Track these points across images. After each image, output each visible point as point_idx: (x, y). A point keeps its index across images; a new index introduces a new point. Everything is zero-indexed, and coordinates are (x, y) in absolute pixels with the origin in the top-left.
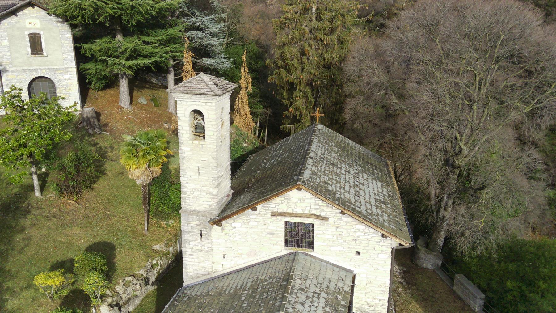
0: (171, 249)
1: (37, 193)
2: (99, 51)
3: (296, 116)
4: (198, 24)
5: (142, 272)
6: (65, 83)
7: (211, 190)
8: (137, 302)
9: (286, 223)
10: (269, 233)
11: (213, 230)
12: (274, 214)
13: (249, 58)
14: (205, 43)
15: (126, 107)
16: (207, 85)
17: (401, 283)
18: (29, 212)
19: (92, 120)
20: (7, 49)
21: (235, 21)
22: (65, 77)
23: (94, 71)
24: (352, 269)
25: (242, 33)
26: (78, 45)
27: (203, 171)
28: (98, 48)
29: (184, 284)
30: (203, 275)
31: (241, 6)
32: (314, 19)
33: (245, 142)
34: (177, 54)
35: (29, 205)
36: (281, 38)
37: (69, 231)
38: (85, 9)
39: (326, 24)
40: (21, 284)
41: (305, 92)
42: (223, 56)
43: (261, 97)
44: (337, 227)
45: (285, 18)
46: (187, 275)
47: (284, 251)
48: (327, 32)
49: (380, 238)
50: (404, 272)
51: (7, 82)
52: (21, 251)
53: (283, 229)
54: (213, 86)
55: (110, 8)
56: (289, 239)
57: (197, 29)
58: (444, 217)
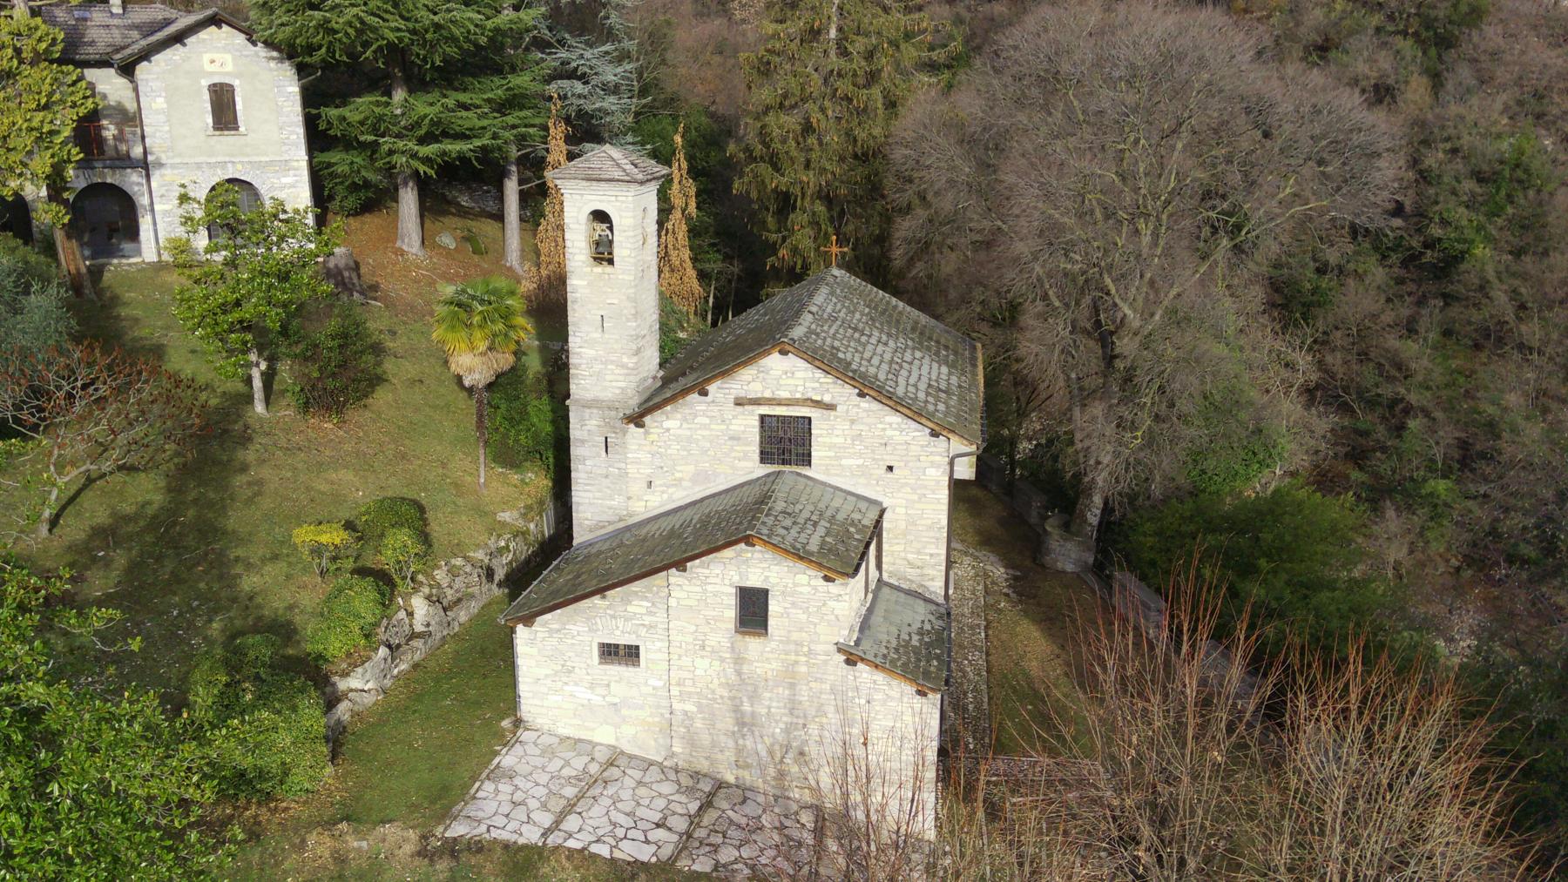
0: (532, 526)
1: (259, 407)
2: (362, 123)
3: (794, 268)
4: (574, 64)
5: (480, 555)
8: (474, 607)
9: (763, 418)
10: (732, 438)
11: (628, 436)
12: (739, 402)
13: (690, 144)
14: (589, 107)
15: (414, 250)
16: (618, 165)
17: (1007, 595)
18: (250, 439)
19: (346, 274)
20: (162, 118)
21: (656, 60)
22: (284, 180)
23: (346, 168)
25: (670, 87)
26: (314, 111)
27: (615, 317)
28: (358, 117)
29: (575, 543)
31: (668, 23)
32: (833, 54)
33: (683, 329)
34: (531, 130)
35: (247, 427)
36: (765, 94)
38: (336, 32)
39: (859, 64)
40: (260, 553)
41: (814, 214)
42: (629, 138)
43: (717, 234)
44: (853, 422)
45: (768, 51)
46: (580, 525)
47: (763, 470)
48: (861, 81)
49: (928, 438)
50: (1016, 578)
51: (163, 191)
52: (250, 501)
53: (757, 430)
54: (629, 167)
55: (392, 29)
57: (572, 75)
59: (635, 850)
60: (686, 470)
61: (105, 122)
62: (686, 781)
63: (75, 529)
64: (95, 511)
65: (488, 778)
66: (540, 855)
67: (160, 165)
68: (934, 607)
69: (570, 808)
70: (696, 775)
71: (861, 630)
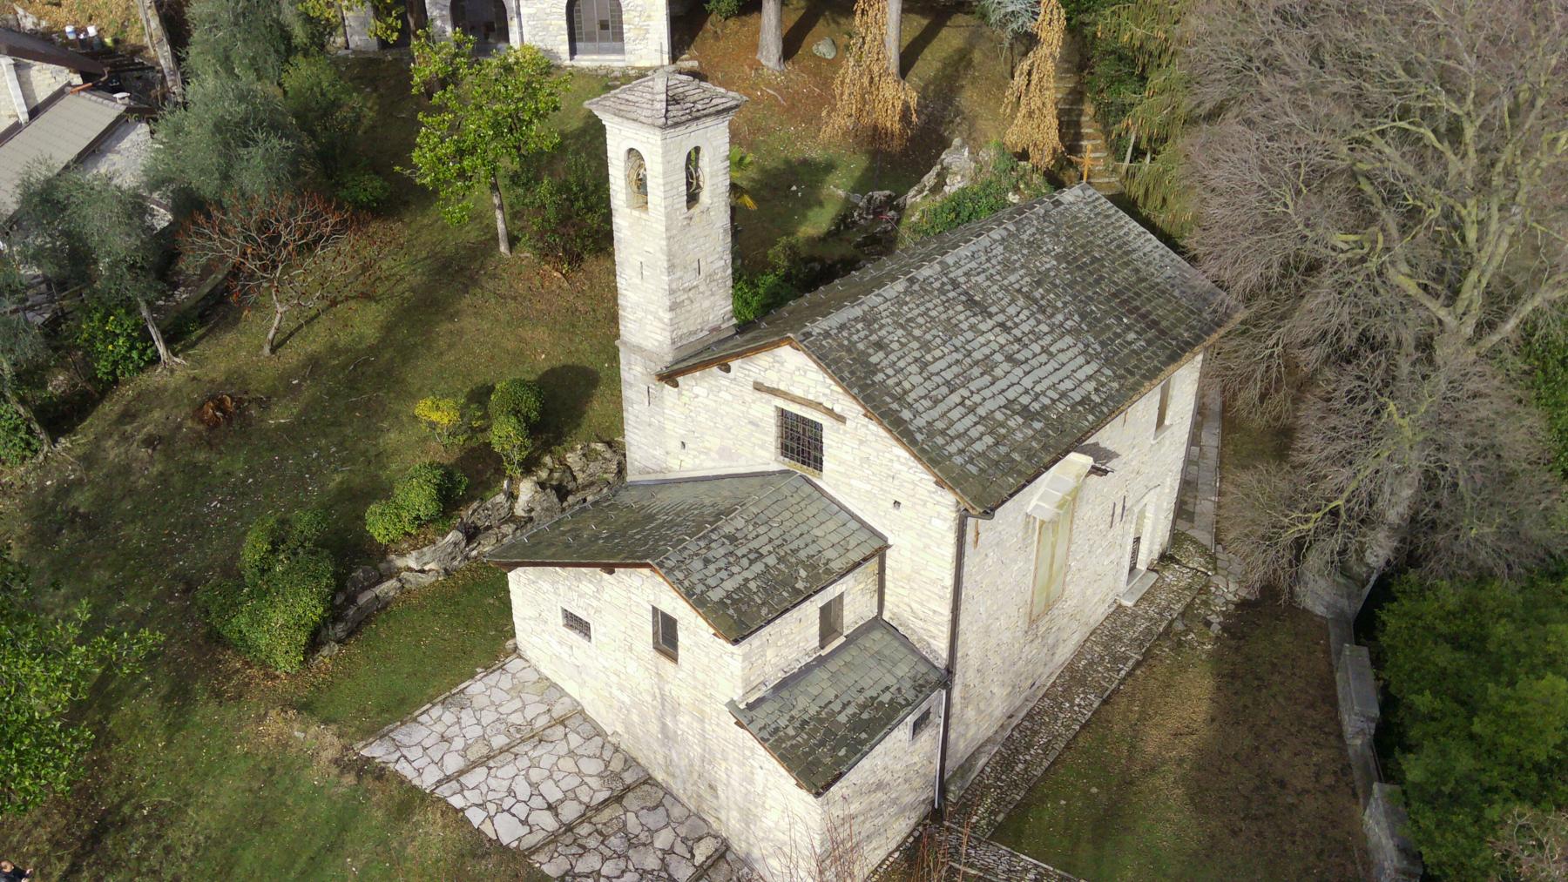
1: (503, 248)
7: (661, 313)
12: (758, 387)
24: (886, 533)
30: (655, 472)
33: (1016, 190)
37: (527, 333)
44: (861, 442)
56: (789, 443)
59: (507, 831)
60: (713, 442)
62: (616, 765)
63: (293, 354)
64: (314, 342)
66: (423, 800)
68: (923, 669)
69: (484, 761)
70: (630, 762)
71: (778, 688)
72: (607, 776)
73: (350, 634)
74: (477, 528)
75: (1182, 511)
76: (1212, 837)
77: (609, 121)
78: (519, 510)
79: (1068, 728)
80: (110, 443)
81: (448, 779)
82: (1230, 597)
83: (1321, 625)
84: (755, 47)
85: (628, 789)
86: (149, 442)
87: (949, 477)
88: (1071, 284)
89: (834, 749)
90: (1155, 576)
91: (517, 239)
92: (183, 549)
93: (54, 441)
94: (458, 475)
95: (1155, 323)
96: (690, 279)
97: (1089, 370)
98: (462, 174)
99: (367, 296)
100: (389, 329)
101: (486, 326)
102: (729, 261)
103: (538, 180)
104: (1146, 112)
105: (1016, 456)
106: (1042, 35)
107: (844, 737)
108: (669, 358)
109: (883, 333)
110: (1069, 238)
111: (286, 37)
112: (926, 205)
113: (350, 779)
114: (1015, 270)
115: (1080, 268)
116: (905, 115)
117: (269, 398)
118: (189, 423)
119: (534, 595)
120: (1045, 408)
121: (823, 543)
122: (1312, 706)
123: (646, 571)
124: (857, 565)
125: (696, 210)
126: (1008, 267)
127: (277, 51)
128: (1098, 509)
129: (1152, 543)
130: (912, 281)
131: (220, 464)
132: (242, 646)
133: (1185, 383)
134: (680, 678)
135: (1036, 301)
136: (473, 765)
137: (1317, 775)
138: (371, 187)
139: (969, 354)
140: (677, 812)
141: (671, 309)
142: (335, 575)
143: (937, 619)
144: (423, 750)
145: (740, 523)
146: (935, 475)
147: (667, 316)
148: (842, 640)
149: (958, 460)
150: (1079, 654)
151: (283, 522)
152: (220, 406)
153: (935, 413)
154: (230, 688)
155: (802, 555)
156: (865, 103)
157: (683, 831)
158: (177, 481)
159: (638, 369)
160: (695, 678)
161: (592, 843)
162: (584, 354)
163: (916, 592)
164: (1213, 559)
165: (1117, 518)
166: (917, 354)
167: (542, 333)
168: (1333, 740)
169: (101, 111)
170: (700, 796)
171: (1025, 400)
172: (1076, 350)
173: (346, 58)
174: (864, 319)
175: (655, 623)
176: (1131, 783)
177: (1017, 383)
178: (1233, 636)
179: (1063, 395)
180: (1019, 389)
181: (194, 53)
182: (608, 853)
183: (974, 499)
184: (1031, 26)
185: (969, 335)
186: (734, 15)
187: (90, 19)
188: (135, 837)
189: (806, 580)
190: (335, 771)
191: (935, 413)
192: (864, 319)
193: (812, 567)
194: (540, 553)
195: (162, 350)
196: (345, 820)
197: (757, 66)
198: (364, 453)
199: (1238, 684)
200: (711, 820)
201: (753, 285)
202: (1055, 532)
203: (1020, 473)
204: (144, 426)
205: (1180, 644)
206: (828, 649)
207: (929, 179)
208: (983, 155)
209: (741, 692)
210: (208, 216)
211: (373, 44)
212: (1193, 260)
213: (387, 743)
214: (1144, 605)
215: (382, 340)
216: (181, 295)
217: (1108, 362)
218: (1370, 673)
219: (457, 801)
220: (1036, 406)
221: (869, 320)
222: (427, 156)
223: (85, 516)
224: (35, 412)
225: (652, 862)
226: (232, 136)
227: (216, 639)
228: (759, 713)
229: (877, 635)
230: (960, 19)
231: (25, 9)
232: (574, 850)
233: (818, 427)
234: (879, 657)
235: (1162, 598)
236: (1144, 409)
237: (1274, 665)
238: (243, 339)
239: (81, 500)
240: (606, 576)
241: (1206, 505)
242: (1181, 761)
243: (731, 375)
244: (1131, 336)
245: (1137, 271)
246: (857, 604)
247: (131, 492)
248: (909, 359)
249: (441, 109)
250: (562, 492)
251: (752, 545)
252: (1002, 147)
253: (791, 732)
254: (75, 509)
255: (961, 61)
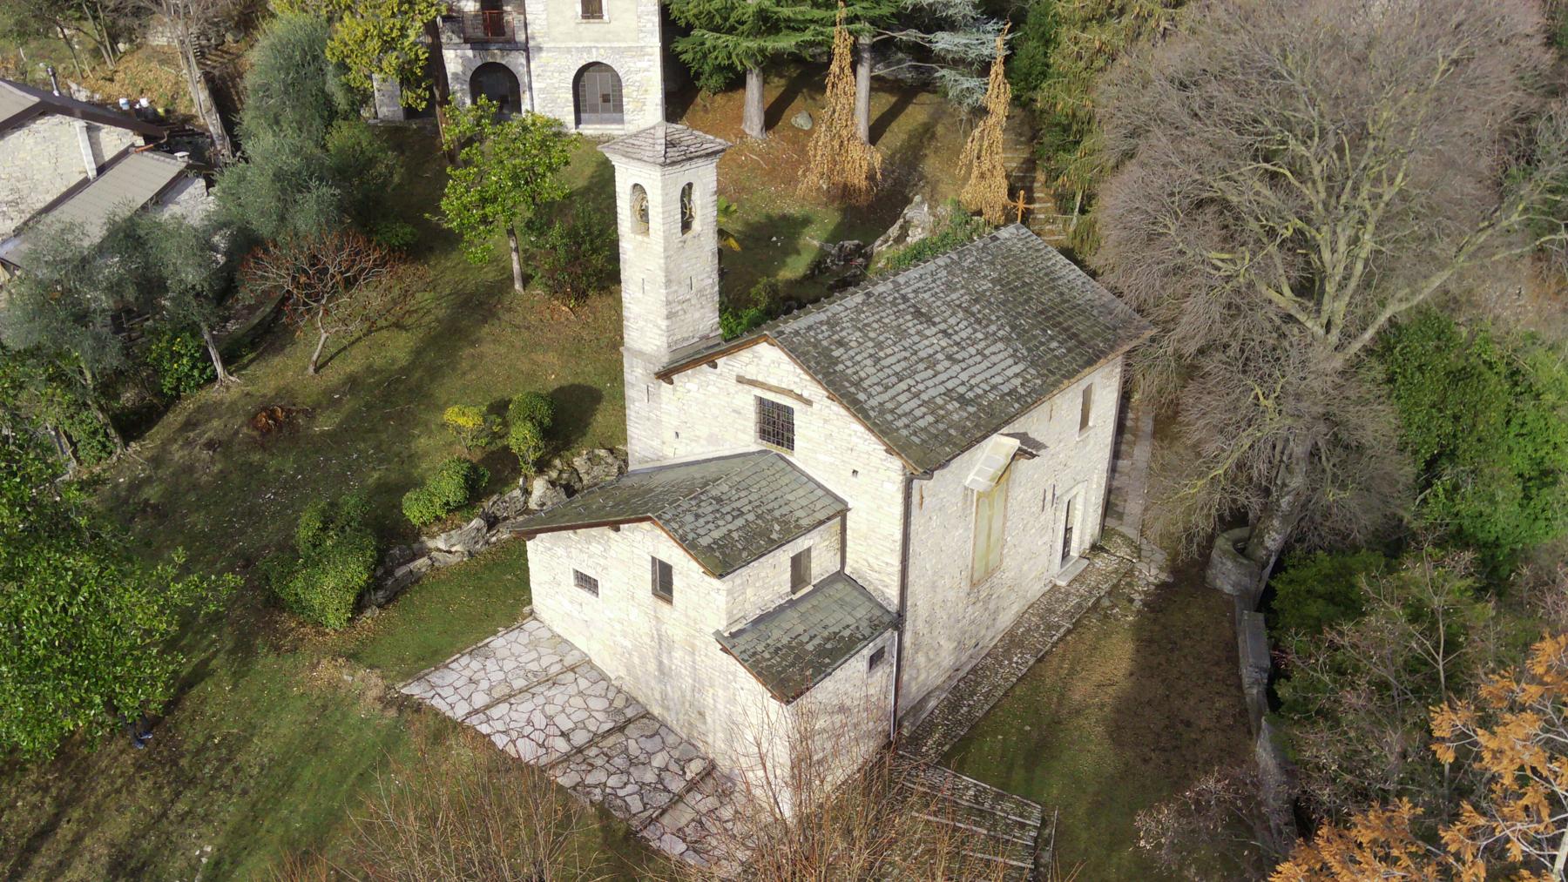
1: (518, 286)
6: (637, 77)
12: (741, 380)
15: (754, 134)
24: (846, 498)
37: (539, 357)
51: (539, 71)
58: (1284, 485)
59: (526, 751)
61: (508, 8)
62: (619, 703)
63: (335, 374)
64: (354, 363)
65: (470, 653)
67: (540, 49)
68: (877, 613)
69: (506, 699)
70: (630, 700)
71: (756, 622)
72: (611, 711)
73: (389, 601)
74: (496, 518)
75: (1109, 508)
76: (1126, 764)
77: (618, 162)
78: (533, 505)
79: (1007, 680)
80: (175, 447)
81: (476, 712)
82: (1151, 579)
83: (1228, 602)
84: (740, 119)
85: (629, 721)
86: (210, 445)
87: (896, 446)
88: (1004, 303)
89: (802, 669)
90: (1086, 562)
91: (531, 277)
92: (242, 532)
93: (127, 445)
94: (482, 469)
95: (1075, 335)
96: (684, 293)
97: (1017, 369)
98: (484, 220)
99: (398, 325)
100: (418, 353)
101: (503, 350)
102: (717, 280)
103: (550, 224)
104: (1074, 164)
105: (952, 432)
106: (991, 106)
107: (811, 661)
108: (665, 360)
109: (844, 333)
110: (1004, 266)
111: (328, 100)
112: (892, 253)
113: (392, 713)
114: (955, 290)
115: (1012, 290)
116: (871, 177)
117: (314, 409)
118: (245, 430)
119: (550, 560)
120: (978, 396)
121: (794, 506)
122: (1217, 664)
123: (646, 525)
124: (821, 523)
125: (689, 235)
126: (950, 287)
127: (322, 117)
128: (1030, 493)
129: (1082, 542)
130: (869, 295)
131: (273, 464)
132: (299, 608)
133: (1105, 386)
134: (673, 618)
135: (973, 315)
136: (497, 702)
137: (1218, 717)
138: (405, 232)
139: (916, 353)
140: (671, 739)
141: (668, 318)
142: (377, 549)
143: (890, 569)
144: (455, 689)
145: (725, 488)
146: (885, 444)
147: (664, 324)
148: (810, 588)
149: (905, 432)
150: (1018, 624)
151: (332, 505)
152: (271, 414)
153: (886, 397)
154: (286, 643)
155: (777, 513)
156: (835, 163)
157: (676, 754)
158: (236, 478)
159: (639, 371)
160: (687, 616)
161: (599, 762)
162: (588, 375)
163: (872, 555)
164: (1138, 550)
165: (1048, 504)
166: (872, 351)
167: (552, 357)
168: (1234, 691)
169: (169, 166)
170: (690, 724)
171: (962, 390)
172: (1006, 354)
173: (375, 126)
174: (828, 323)
175: (654, 572)
176: (1059, 723)
177: (956, 377)
178: (1152, 610)
179: (994, 387)
180: (957, 382)
181: (248, 118)
182: (612, 769)
183: (916, 462)
184: (982, 99)
185: (916, 338)
186: (721, 91)
187: (142, 92)
188: (208, 760)
189: (779, 532)
190: (379, 706)
191: (886, 397)
192: (828, 323)
193: (784, 523)
194: (552, 522)
195: (219, 369)
196: (392, 740)
197: (742, 135)
198: (398, 455)
199: (1155, 647)
200: (700, 745)
201: (737, 317)
202: (991, 506)
203: (955, 444)
204: (205, 432)
205: (1106, 616)
206: (799, 595)
207: (894, 231)
208: (940, 210)
209: (725, 623)
210: (266, 251)
211: (400, 115)
212: (1093, 274)
213: (424, 685)
214: (1077, 585)
215: (413, 362)
216: (232, 326)
217: (1033, 364)
218: (1265, 633)
219: (484, 729)
220: (971, 395)
221: (832, 323)
222: (454, 203)
223: (155, 507)
224: (112, 418)
225: (650, 777)
226: (289, 184)
227: (275, 603)
228: (740, 640)
229: (840, 586)
230: (925, 97)
231: (79, 84)
232: (584, 767)
233: (790, 411)
234: (842, 603)
235: (1092, 580)
236: (1066, 403)
237: (1186, 633)
238: (290, 362)
239: (152, 493)
240: (612, 534)
241: (1133, 507)
242: (1102, 706)
243: (718, 371)
244: (1054, 344)
245: (1062, 294)
246: (822, 564)
247: (195, 486)
248: (865, 355)
249: (467, 163)
250: (570, 491)
251: (735, 505)
252: (958, 204)
253: (767, 655)
254: (146, 501)
255: (926, 133)
